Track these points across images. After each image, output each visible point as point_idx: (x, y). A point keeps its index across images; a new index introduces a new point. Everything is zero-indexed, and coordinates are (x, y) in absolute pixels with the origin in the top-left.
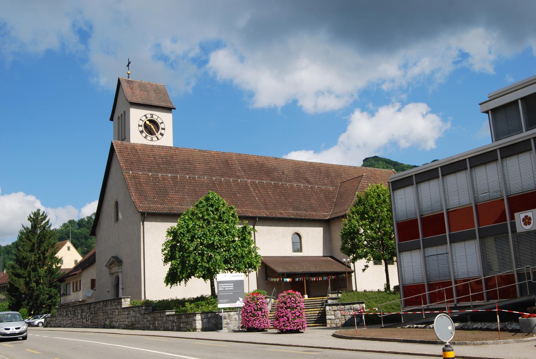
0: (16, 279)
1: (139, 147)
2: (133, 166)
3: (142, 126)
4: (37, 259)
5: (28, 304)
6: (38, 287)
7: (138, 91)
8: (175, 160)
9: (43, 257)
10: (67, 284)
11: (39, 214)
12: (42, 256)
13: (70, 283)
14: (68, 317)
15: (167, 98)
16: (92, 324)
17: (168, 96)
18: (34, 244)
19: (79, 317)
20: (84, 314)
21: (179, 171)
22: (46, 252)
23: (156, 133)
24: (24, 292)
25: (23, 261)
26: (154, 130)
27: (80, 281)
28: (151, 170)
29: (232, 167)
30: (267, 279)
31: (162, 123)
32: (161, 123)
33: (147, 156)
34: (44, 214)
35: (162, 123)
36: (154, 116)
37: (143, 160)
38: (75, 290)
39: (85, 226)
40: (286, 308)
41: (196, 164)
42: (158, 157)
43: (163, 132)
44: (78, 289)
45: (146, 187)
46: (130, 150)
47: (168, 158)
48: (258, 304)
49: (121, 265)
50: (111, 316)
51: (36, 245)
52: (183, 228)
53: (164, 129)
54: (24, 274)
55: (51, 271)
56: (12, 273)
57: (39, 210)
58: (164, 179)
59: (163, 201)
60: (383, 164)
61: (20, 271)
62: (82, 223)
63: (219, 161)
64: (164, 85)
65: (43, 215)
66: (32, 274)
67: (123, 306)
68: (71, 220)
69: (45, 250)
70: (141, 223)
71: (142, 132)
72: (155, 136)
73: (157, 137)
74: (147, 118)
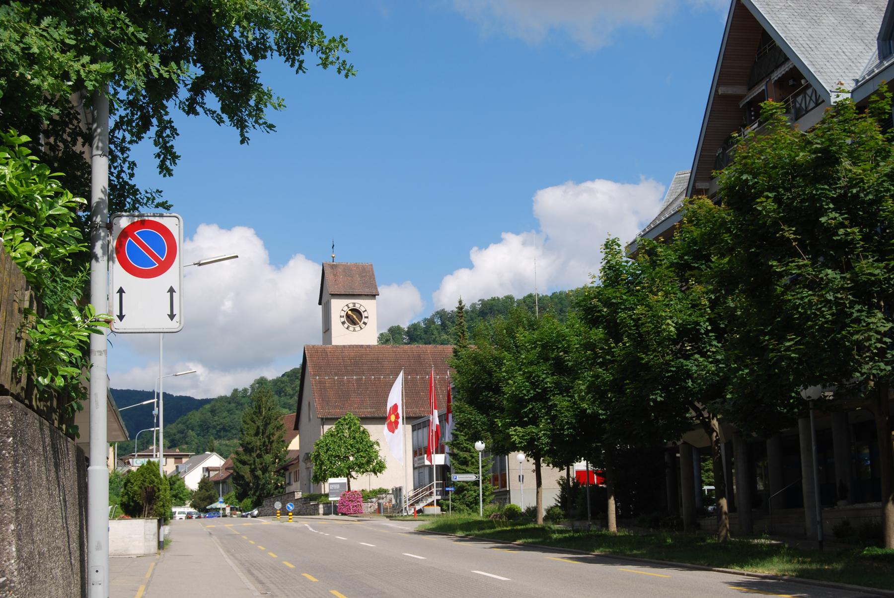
3: (343, 316)
5: (254, 494)
12: (267, 441)
18: (258, 427)
22: (271, 436)
31: (366, 311)
32: (364, 312)
35: (366, 311)
36: (357, 305)
39: (421, 339)
51: (261, 428)
53: (367, 317)
54: (249, 461)
56: (237, 459)
62: (415, 333)
66: (257, 460)
67: (296, 498)
68: (393, 327)
69: (270, 434)
71: (343, 323)
74: (349, 308)
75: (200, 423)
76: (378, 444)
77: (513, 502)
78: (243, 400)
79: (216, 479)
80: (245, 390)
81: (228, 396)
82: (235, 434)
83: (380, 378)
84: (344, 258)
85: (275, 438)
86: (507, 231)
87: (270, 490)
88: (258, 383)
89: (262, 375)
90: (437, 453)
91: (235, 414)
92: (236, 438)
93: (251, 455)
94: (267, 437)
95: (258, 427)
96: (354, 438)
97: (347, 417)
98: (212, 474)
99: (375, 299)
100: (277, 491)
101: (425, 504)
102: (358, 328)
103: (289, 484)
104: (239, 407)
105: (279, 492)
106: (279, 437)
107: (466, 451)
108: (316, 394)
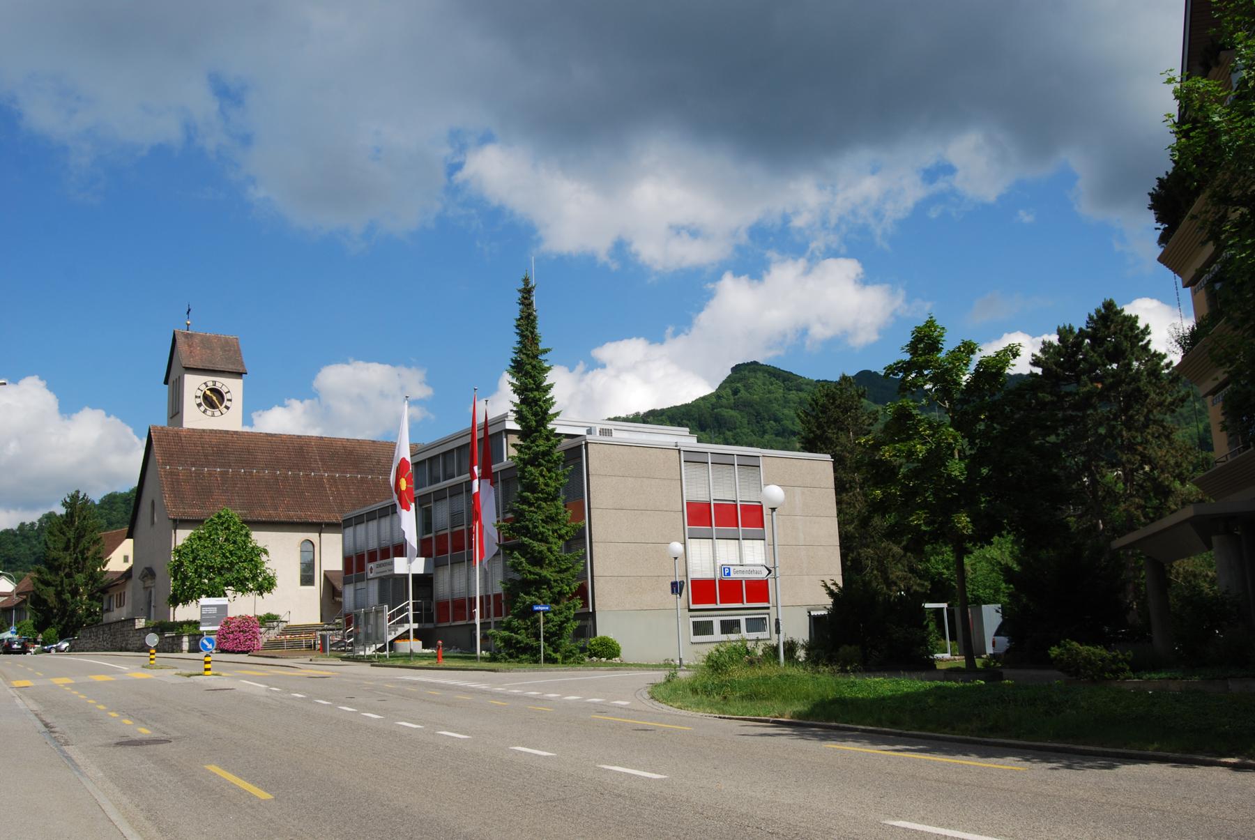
0: (43, 587)
1: (185, 433)
3: (200, 397)
5: (59, 623)
7: (199, 348)
11: (79, 497)
13: (113, 595)
17: (240, 354)
19: (101, 639)
20: (105, 635)
21: (233, 464)
22: (86, 552)
23: (219, 406)
26: (216, 401)
27: (124, 593)
30: (333, 598)
31: (229, 392)
32: (226, 393)
34: (85, 498)
35: (229, 392)
40: (240, 632)
42: (208, 446)
43: (228, 404)
44: (122, 604)
49: (154, 578)
51: (72, 540)
54: (54, 581)
55: (93, 578)
57: (78, 492)
60: (764, 377)
64: (236, 338)
65: (83, 498)
66: (66, 581)
67: (137, 627)
69: (84, 549)
70: (173, 531)
71: (199, 405)
74: (207, 386)
76: (266, 552)
77: (600, 633)
80: (33, 524)
83: (252, 472)
84: (202, 326)
85: (90, 554)
87: (81, 617)
89: (51, 510)
92: (21, 570)
93: (57, 574)
96: (235, 542)
97: (223, 514)
99: (242, 379)
100: (90, 618)
101: (395, 637)
102: (217, 413)
103: (108, 610)
104: (26, 540)
105: (93, 620)
106: (96, 553)
107: (541, 541)
108: (166, 489)
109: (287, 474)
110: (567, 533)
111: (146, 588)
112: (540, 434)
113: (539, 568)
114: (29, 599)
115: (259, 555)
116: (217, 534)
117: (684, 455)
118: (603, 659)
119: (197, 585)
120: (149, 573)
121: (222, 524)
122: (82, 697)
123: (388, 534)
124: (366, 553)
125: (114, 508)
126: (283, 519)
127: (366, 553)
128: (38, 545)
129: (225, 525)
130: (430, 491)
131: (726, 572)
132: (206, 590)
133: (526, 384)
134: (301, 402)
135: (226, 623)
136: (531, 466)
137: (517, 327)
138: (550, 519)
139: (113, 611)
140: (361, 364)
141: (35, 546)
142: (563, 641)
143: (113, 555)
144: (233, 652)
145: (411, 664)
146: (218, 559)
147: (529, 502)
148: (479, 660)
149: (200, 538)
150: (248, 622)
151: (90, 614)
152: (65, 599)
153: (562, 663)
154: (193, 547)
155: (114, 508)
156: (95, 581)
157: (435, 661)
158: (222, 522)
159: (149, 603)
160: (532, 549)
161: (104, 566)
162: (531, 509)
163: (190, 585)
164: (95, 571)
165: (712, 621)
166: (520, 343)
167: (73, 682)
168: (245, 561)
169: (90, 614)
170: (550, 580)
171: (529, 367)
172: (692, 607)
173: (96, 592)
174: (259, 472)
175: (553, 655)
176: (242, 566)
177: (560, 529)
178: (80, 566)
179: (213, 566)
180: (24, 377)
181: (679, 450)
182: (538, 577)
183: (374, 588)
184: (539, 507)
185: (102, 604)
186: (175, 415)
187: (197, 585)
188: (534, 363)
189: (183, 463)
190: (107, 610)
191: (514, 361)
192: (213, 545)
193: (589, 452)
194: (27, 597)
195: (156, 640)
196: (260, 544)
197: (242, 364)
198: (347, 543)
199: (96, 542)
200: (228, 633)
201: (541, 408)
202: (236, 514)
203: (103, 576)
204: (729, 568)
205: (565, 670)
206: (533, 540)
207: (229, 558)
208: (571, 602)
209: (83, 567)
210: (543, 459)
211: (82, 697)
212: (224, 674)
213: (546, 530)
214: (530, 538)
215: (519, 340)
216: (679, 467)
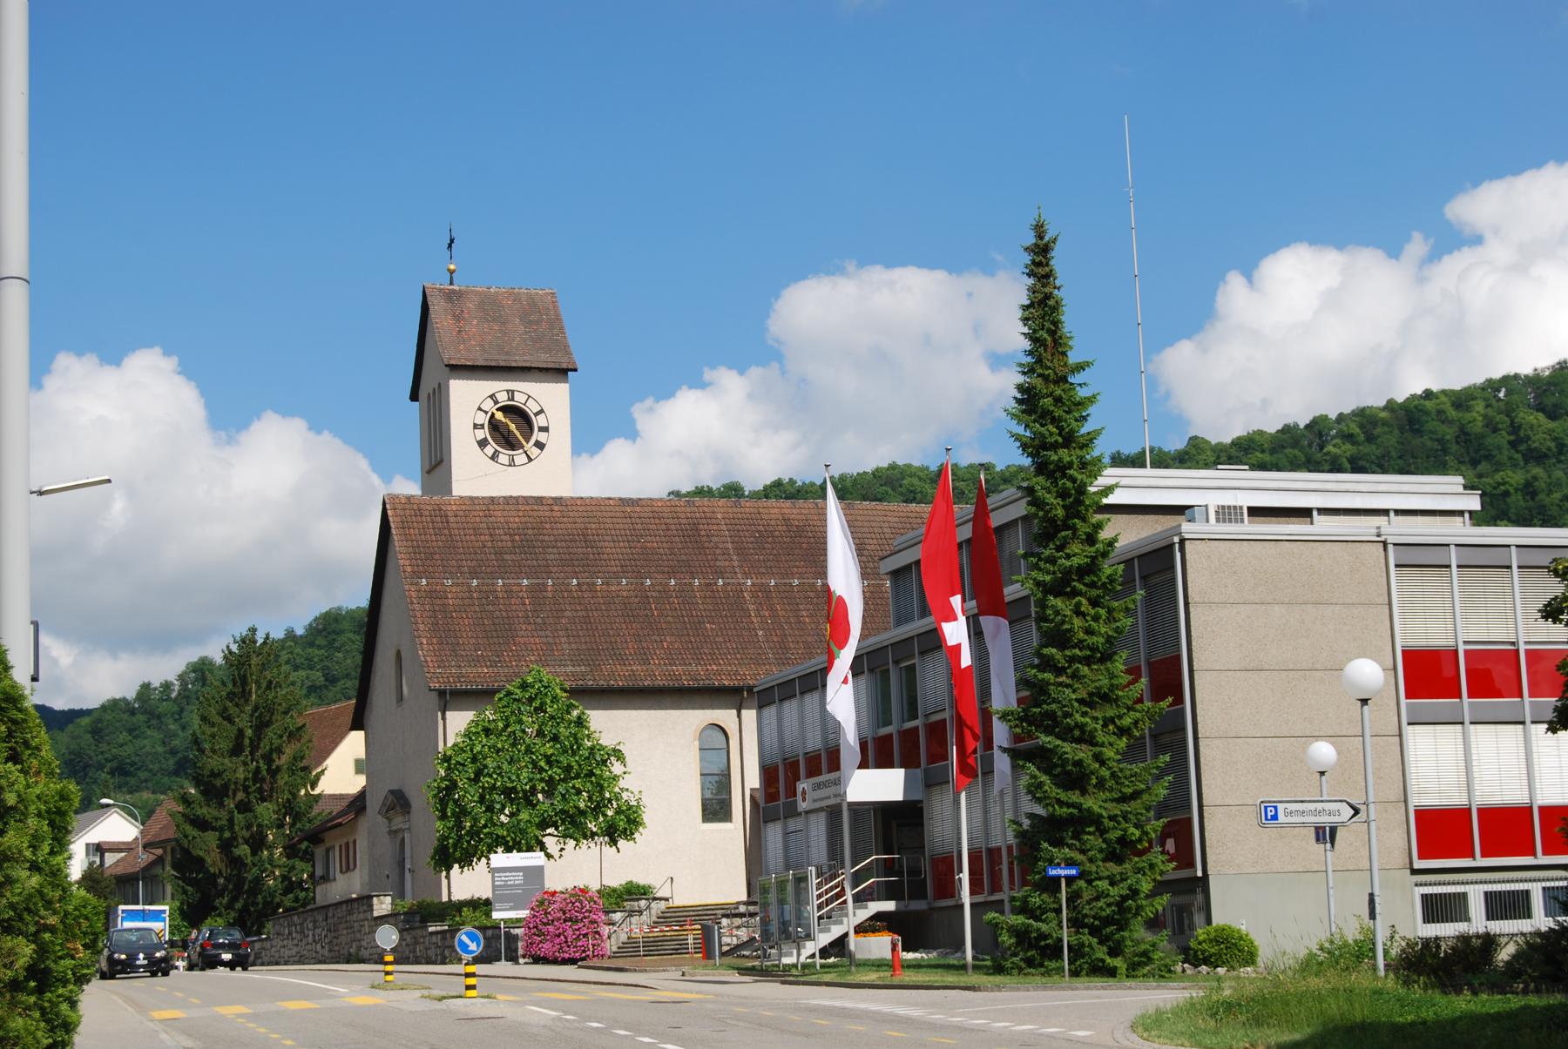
0: (195, 833)
1: (454, 508)
2: (431, 563)
3: (482, 426)
4: (251, 775)
5: (229, 907)
6: (257, 858)
8: (546, 538)
9: (269, 770)
10: (328, 851)
11: (255, 642)
12: (264, 767)
13: (333, 847)
14: (293, 939)
15: (557, 335)
16: (332, 954)
17: (562, 328)
19: (310, 939)
20: (318, 931)
22: (275, 756)
23: (524, 442)
24: (217, 871)
25: (214, 782)
27: (355, 842)
28: (478, 570)
29: (706, 545)
31: (542, 411)
32: (536, 414)
33: (471, 532)
35: (542, 411)
36: (517, 396)
37: (460, 544)
38: (344, 870)
40: (565, 921)
41: (607, 544)
42: (502, 532)
43: (542, 437)
45: (460, 621)
46: (429, 519)
47: (530, 532)
48: (549, 913)
49: (409, 812)
50: (358, 935)
51: (249, 732)
52: (464, 751)
53: (545, 429)
54: (216, 819)
56: (184, 815)
57: (253, 630)
58: (509, 592)
59: (498, 656)
61: (205, 810)
63: (673, 527)
64: (553, 294)
65: (265, 643)
66: (239, 818)
67: (376, 914)
70: (439, 714)
71: (482, 444)
72: (521, 451)
73: (525, 452)
74: (496, 402)
75: (67, 756)
76: (618, 755)
77: (1218, 919)
78: (164, 707)
79: (120, 871)
80: (167, 686)
81: (129, 698)
82: (146, 781)
83: (594, 584)
85: (283, 760)
86: (713, 367)
87: (272, 895)
88: (194, 671)
90: (863, 765)
91: (145, 738)
92: (147, 788)
93: (221, 805)
94: (263, 757)
95: (241, 732)
96: (555, 739)
97: (530, 680)
98: (110, 859)
99: (566, 381)
102: (520, 458)
103: (326, 878)
104: (154, 722)
105: (296, 900)
106: (295, 758)
107: (1079, 741)
108: (422, 627)
109: (667, 584)
110: (1136, 723)
111: (393, 833)
112: (1074, 534)
113: (1077, 792)
114: (169, 858)
115: (604, 762)
116: (520, 722)
117: (1395, 551)
118: (1219, 969)
119: (485, 826)
120: (399, 802)
121: (531, 700)
122: (262, 1030)
123: (775, 740)
124: (801, 758)
125: (337, 644)
126: (660, 683)
127: (801, 758)
128: (180, 732)
129: (537, 703)
130: (885, 644)
131: (1269, 814)
132: (503, 837)
133: (1042, 435)
134: (741, 372)
135: (542, 903)
136: (1055, 597)
137: (1025, 320)
138: (1103, 697)
139: (335, 879)
140: (877, 274)
141: (175, 735)
142: (1126, 934)
143: (329, 762)
144: (555, 962)
145: (849, 979)
146: (524, 775)
147: (1055, 665)
148: (970, 970)
149: (487, 731)
150: (581, 902)
151: (290, 886)
152: (239, 856)
153: (1127, 977)
154: (475, 751)
155: (337, 644)
156: (297, 817)
157: (840, 974)
158: (530, 697)
159: (401, 864)
160: (1060, 758)
161: (314, 785)
162: (1061, 680)
163: (471, 827)
164: (295, 795)
165: (1527, 892)
166: (1030, 353)
167: (251, 1011)
168: (577, 776)
169: (290, 886)
170: (1101, 816)
171: (1048, 401)
172: (1418, 864)
173: (300, 842)
174: (607, 584)
175: (1109, 960)
176: (574, 787)
177: (1120, 717)
178: (265, 787)
179: (515, 788)
180: (134, 350)
181: (1385, 544)
182: (1075, 811)
183: (818, 829)
184: (1075, 676)
185: (313, 866)
186: (436, 466)
187: (485, 826)
188: (1058, 392)
189: (453, 570)
190: (322, 878)
191: (1020, 388)
192: (514, 745)
193: (1187, 557)
194: (165, 852)
195: (394, 937)
196: (607, 741)
197: (566, 349)
198: (767, 740)
199: (294, 734)
200: (545, 924)
201: (1074, 480)
202: (554, 677)
203: (311, 807)
204: (1276, 808)
205: (1103, 988)
206: (1064, 740)
207: (546, 771)
208: (1144, 858)
209: (272, 789)
210: (1080, 580)
211: (262, 1030)
212: (499, 997)
213: (1090, 720)
214: (1058, 737)
215: (1029, 348)
216: (1385, 579)
